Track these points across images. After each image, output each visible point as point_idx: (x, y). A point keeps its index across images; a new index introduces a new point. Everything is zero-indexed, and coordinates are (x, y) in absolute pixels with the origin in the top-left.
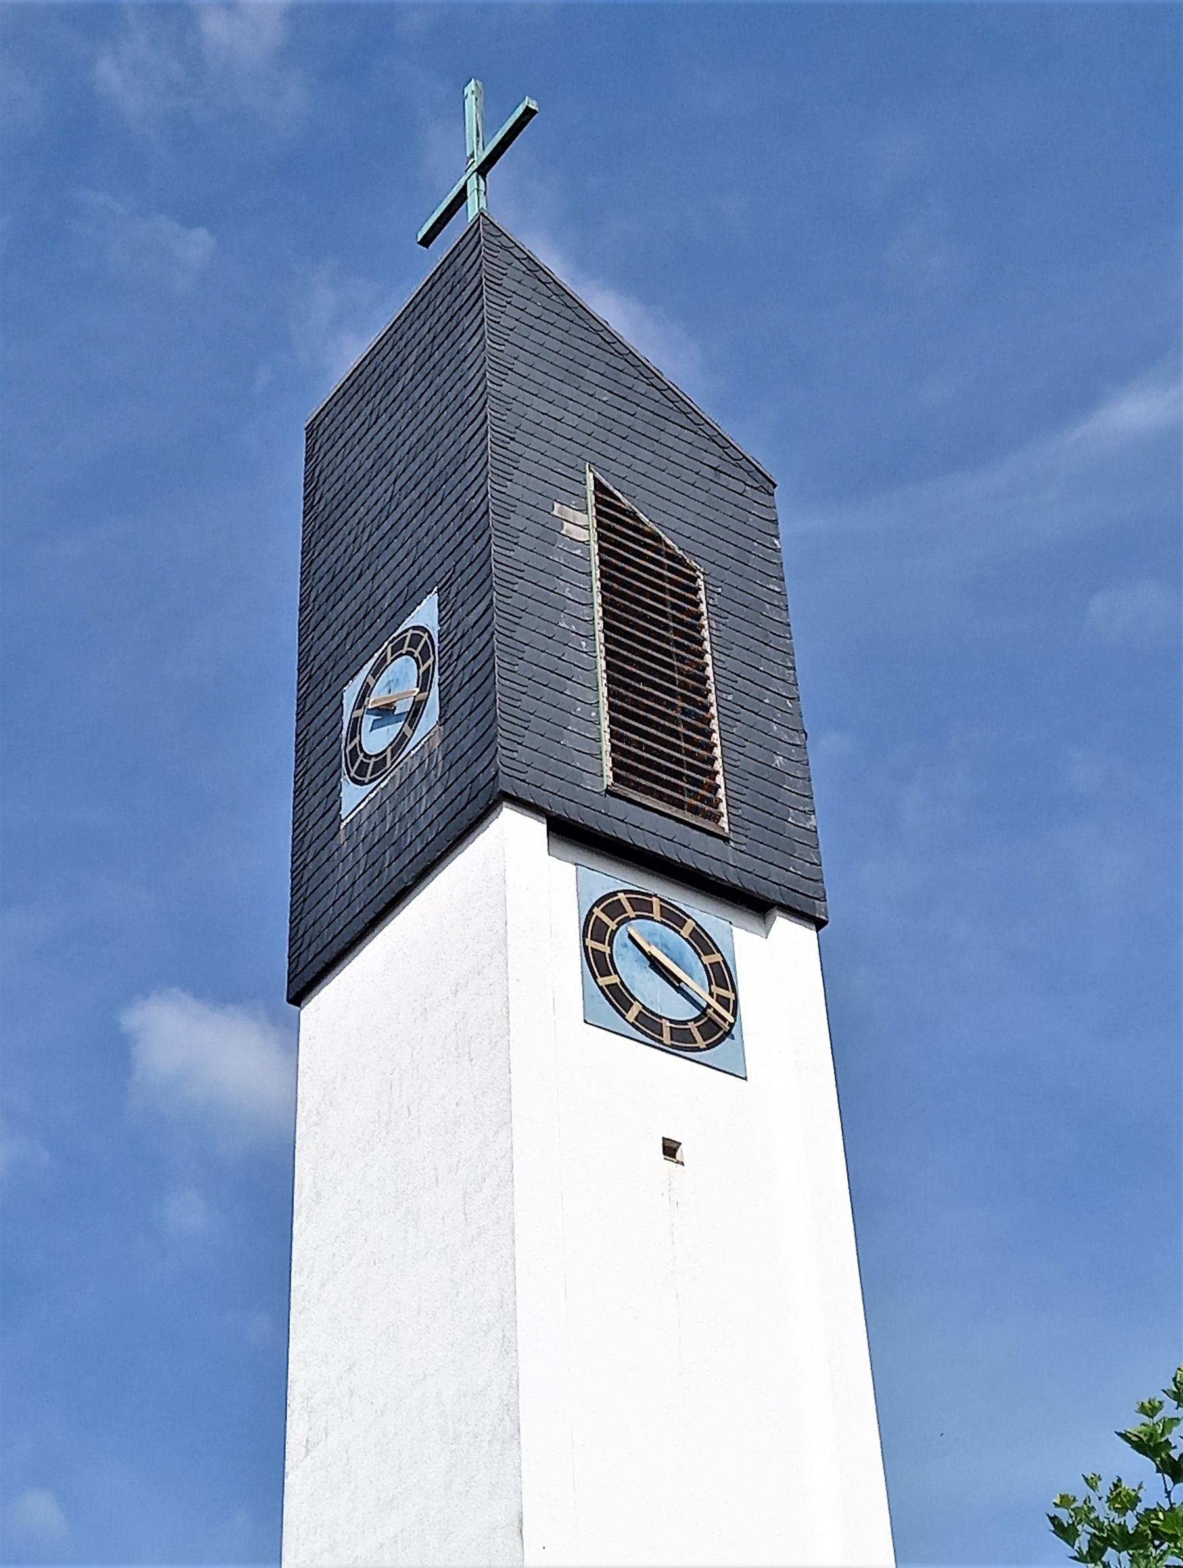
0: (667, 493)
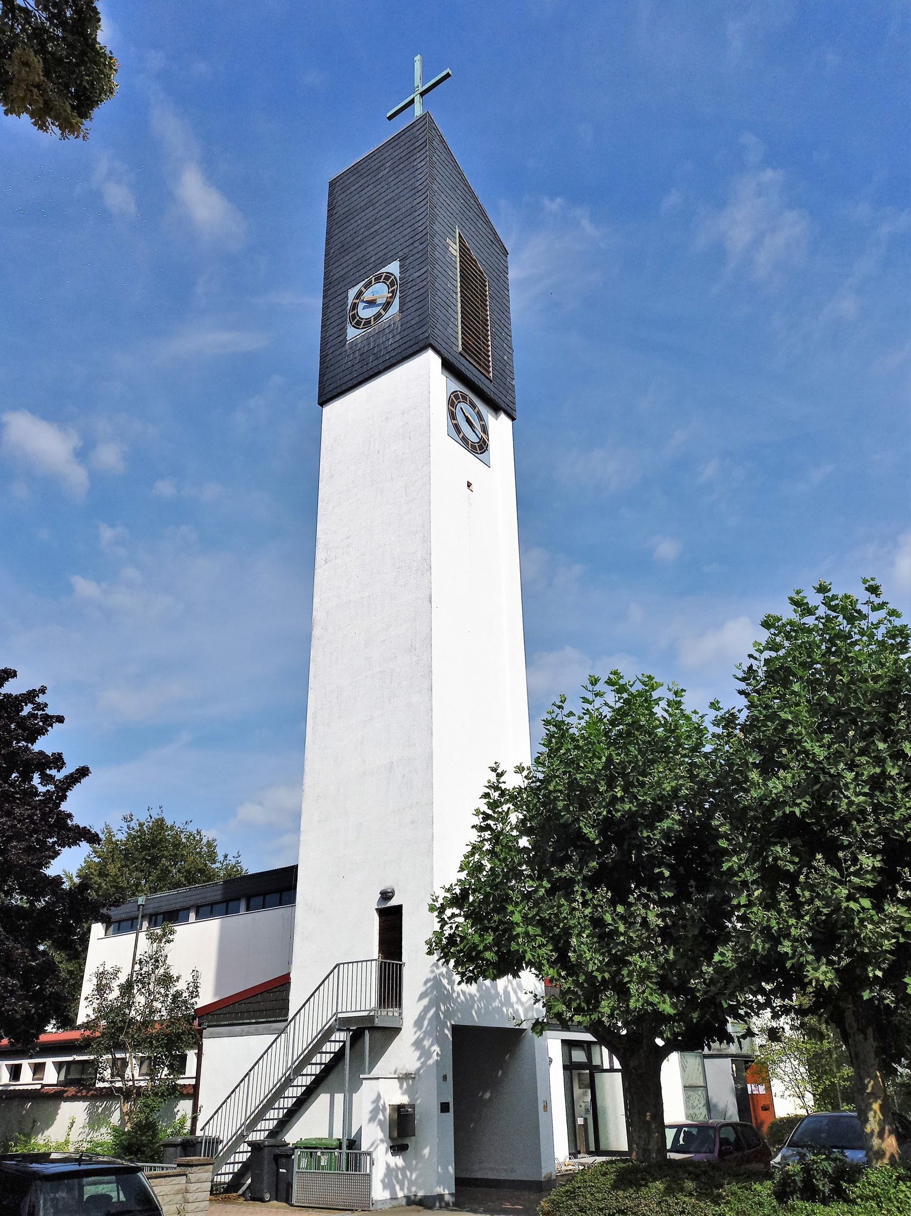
0: (478, 246)
